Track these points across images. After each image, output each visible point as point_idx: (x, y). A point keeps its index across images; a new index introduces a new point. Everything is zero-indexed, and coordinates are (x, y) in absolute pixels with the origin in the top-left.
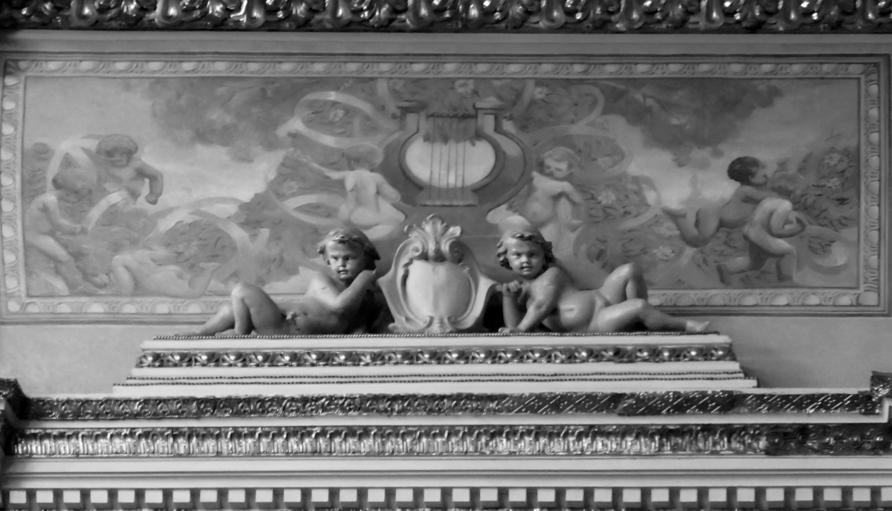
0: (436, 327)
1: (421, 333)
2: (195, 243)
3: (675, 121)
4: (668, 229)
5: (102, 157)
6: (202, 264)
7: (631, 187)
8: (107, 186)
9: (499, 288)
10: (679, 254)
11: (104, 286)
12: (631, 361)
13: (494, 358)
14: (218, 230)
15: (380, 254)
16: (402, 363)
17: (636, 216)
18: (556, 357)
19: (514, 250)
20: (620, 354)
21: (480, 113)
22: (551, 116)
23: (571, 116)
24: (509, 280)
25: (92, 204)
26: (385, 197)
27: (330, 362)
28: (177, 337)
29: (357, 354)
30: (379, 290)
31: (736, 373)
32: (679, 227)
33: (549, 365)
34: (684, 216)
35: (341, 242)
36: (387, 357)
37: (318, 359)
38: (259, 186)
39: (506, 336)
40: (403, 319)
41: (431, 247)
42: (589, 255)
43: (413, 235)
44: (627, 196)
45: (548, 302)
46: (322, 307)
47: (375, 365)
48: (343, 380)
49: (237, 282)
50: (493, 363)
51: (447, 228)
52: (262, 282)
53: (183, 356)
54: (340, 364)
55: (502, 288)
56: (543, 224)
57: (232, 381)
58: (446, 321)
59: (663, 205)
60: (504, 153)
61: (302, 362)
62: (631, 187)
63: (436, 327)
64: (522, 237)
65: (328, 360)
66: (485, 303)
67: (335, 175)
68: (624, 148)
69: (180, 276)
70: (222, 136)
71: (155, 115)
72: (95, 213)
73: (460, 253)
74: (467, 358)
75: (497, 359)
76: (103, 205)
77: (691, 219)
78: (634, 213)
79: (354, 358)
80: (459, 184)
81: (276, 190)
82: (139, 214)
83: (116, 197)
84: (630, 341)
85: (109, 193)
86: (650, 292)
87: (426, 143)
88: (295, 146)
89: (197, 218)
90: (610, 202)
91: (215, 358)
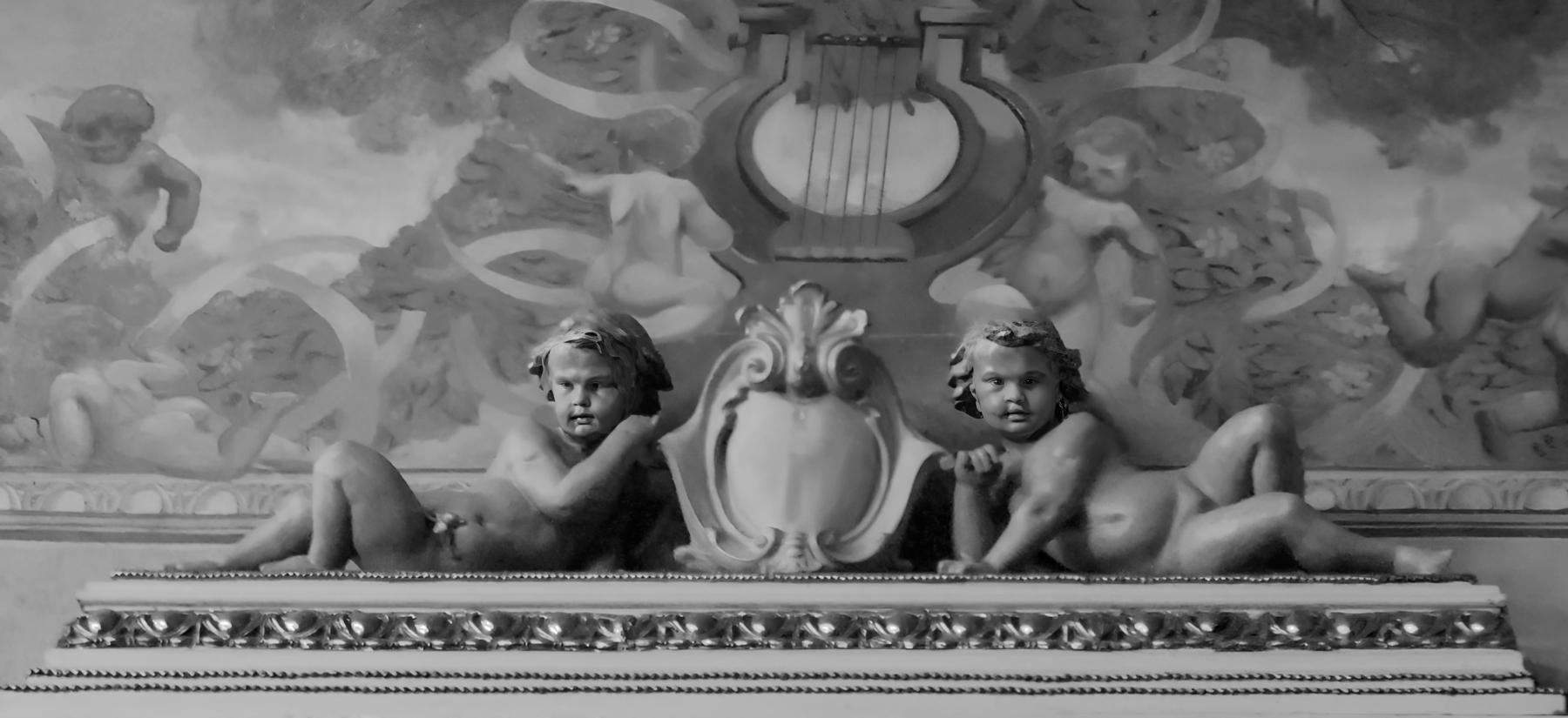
0: (786, 559)
1: (752, 572)
2: (248, 345)
3: (1386, 55)
4: (1360, 320)
5: (74, 138)
6: (256, 396)
7: (1277, 216)
8: (73, 207)
9: (945, 463)
10: (1384, 382)
11: (21, 447)
12: (1256, 646)
13: (922, 635)
14: (309, 313)
15: (674, 383)
16: (1150, 646)
17: (1286, 288)
18: (1072, 634)
19: (989, 369)
20: (1230, 630)
21: (931, 34)
22: (1094, 41)
23: (1145, 44)
24: (970, 446)
25: (32, 249)
26: (699, 239)
27: (524, 641)
28: (170, 573)
29: (591, 621)
30: (663, 466)
31: (1514, 677)
32: (1386, 317)
33: (250, 652)
34: (1400, 289)
35: (585, 345)
36: (662, 630)
37: (497, 634)
38: (415, 211)
39: (957, 580)
40: (712, 536)
41: (795, 360)
42: (1168, 386)
43: (755, 331)
44: (1266, 240)
45: (1063, 497)
46: (521, 501)
47: (634, 648)
48: (549, 684)
49: (329, 442)
50: (919, 646)
51: (834, 315)
52: (389, 438)
53: (175, 620)
54: (548, 646)
55: (954, 463)
56: (1063, 306)
57: (282, 683)
58: (812, 541)
59: (1348, 263)
60: (982, 132)
61: (457, 639)
62: (1277, 216)
63: (786, 559)
64: (1010, 340)
65: (518, 635)
66: (912, 495)
67: (588, 184)
68: (1263, 119)
69: (202, 425)
70: (347, 91)
71: (200, 41)
72: (36, 272)
73: (861, 377)
74: (856, 634)
75: (928, 638)
76: (57, 251)
77: (1417, 297)
78: (1281, 281)
79: (582, 632)
80: (872, 210)
81: (450, 218)
82: (133, 273)
83: (89, 234)
84: (1254, 596)
85: (74, 223)
86: (1310, 476)
87: (802, 107)
88: (504, 115)
89: (262, 285)
90: (1223, 253)
91: (250, 628)
